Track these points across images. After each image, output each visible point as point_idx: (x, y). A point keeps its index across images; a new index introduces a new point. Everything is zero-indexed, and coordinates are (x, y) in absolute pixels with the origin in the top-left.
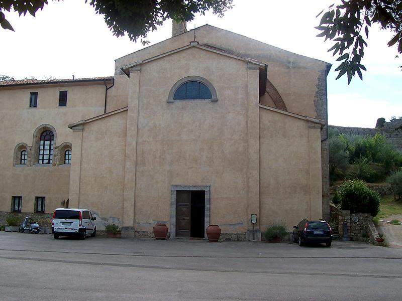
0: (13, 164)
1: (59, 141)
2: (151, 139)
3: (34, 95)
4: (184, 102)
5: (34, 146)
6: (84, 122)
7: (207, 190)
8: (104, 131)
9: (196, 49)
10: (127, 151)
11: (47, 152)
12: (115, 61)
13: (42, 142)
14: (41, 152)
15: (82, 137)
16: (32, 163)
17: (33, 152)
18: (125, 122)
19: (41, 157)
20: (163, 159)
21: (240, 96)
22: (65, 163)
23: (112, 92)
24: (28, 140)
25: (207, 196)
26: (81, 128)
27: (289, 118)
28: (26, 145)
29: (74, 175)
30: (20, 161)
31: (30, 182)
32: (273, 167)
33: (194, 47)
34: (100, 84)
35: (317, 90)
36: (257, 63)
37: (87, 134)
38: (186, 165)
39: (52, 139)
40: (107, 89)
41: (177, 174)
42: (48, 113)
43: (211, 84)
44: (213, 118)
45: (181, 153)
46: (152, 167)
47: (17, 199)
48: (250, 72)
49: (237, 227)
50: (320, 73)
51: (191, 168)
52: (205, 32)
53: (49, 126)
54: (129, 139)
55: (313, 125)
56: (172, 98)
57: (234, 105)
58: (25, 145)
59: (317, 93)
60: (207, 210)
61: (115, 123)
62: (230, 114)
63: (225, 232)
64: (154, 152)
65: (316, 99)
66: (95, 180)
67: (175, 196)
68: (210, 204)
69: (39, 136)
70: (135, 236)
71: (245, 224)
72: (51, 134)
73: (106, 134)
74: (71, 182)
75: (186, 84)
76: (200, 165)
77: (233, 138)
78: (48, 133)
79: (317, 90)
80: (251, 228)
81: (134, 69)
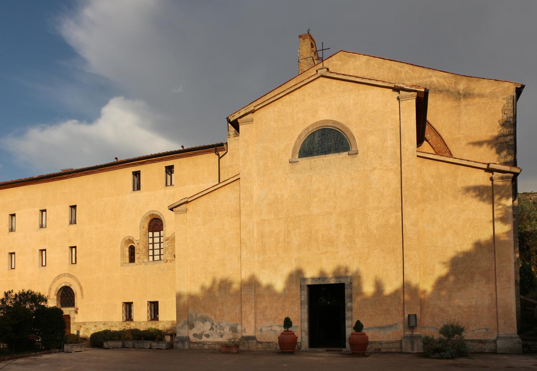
4: (312, 160)
6: (186, 200)
8: (213, 211)
13: (151, 234)
14: (151, 247)
21: (389, 143)
24: (136, 230)
25: (347, 292)
28: (133, 238)
30: (132, 259)
32: (439, 245)
34: (210, 152)
40: (220, 158)
43: (347, 129)
44: (352, 179)
47: (128, 306)
50: (505, 102)
52: (339, 63)
54: (244, 219)
56: (297, 156)
58: (131, 239)
60: (348, 311)
61: (227, 195)
62: (376, 171)
63: (373, 340)
64: (277, 234)
67: (305, 293)
68: (352, 302)
71: (401, 327)
75: (313, 134)
80: (408, 333)
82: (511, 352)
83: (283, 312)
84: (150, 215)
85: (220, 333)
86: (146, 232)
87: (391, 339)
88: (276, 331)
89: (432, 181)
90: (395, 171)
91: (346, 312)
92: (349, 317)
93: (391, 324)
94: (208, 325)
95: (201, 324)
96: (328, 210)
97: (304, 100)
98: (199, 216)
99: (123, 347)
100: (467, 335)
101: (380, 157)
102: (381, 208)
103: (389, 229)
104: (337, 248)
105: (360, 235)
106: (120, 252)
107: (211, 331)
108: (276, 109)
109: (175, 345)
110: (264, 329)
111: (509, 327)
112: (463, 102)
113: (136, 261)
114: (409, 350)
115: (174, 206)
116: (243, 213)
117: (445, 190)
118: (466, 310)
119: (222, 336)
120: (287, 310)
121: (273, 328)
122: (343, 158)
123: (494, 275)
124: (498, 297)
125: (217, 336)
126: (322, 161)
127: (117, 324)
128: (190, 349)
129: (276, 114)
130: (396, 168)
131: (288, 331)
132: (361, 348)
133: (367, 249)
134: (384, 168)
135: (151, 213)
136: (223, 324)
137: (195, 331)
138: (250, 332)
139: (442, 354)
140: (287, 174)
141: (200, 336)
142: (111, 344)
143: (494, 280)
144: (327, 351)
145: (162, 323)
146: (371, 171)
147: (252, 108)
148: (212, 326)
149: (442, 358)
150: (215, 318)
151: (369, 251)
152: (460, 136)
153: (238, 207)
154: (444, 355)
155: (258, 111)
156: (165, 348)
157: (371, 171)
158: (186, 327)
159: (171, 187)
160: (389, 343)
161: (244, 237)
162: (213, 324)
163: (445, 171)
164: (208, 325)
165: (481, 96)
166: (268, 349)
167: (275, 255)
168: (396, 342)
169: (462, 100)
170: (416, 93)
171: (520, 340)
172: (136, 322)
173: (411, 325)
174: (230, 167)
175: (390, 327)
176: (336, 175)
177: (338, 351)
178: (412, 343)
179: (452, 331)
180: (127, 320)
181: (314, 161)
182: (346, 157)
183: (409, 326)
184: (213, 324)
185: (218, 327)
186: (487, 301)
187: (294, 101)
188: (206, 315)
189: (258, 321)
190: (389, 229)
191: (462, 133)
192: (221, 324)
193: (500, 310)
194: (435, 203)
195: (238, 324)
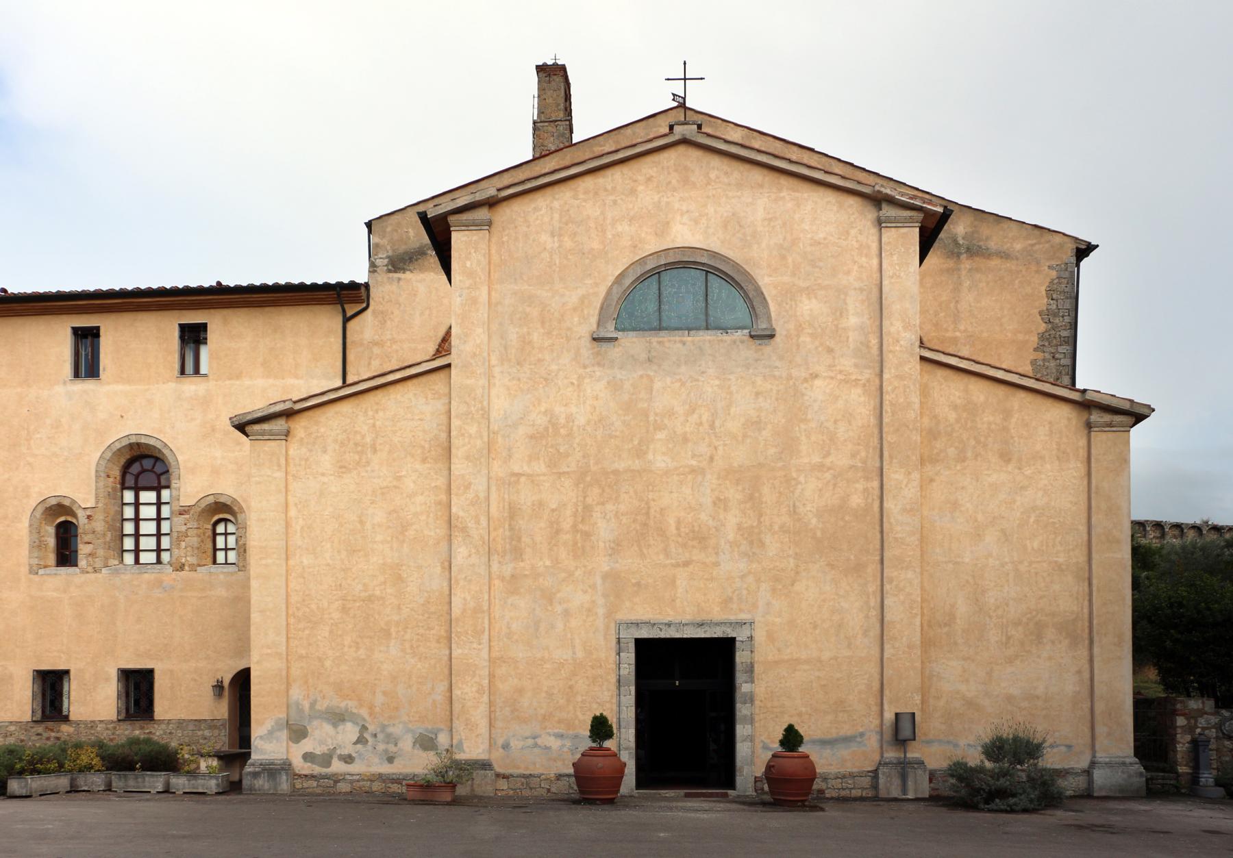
0: (31, 566)
1: (191, 486)
2: (540, 467)
3: (87, 338)
4: (654, 340)
5: (100, 505)
6: (288, 405)
7: (741, 635)
8: (368, 440)
9: (695, 153)
10: (454, 510)
11: (148, 528)
12: (369, 225)
13: (129, 496)
15: (286, 460)
16: (98, 563)
17: (99, 525)
18: (443, 409)
19: (129, 544)
20: (587, 535)
21: (853, 320)
22: (214, 562)
23: (365, 327)
24: (82, 487)
25: (741, 657)
26: (279, 425)
27: (1022, 394)
28: (74, 502)
29: (265, 595)
30: (66, 555)
31: (99, 626)
32: (967, 560)
33: (685, 141)
35: (1043, 327)
36: (918, 203)
37: (304, 450)
38: (667, 555)
39: (163, 483)
40: (346, 320)
41: (638, 584)
42: (141, 391)
43: (746, 274)
44: (757, 394)
45: (647, 514)
46: (548, 563)
47: (51, 685)
48: (889, 235)
49: (844, 752)
50: (1054, 274)
51: (687, 564)
53: (152, 442)
54: (459, 467)
55: (1107, 418)
57: (830, 351)
58: (67, 503)
59: (1042, 337)
62: (818, 382)
64: (553, 510)
65: (1040, 355)
66: (344, 610)
67: (630, 657)
68: (752, 682)
69: (116, 472)
70: (109, 789)
71: (873, 742)
72: (158, 469)
73: (375, 451)
74: (255, 617)
76: (717, 554)
77: (828, 461)
78: (147, 463)
79: (1043, 327)
80: (891, 754)
81: (465, 217)
82: (1124, 795)
83: (568, 701)
84: (131, 446)
85: (386, 751)
86: (114, 489)
87: (850, 768)
88: (547, 748)
89: (952, 416)
90: (864, 385)
91: (738, 706)
92: (745, 716)
93: (849, 733)
94: (350, 732)
95: (328, 728)
96: (694, 463)
97: (633, 192)
98: (325, 452)
99: (74, 790)
100: (1051, 760)
101: (830, 351)
102: (829, 469)
103: (847, 518)
104: (717, 554)
105: (776, 528)
106: (22, 534)
107: (359, 746)
108: (556, 204)
109: (246, 782)
110: (515, 744)
111: (1118, 742)
112: (966, 264)
113: (82, 563)
114: (895, 792)
115: (249, 417)
116: (458, 453)
117: (982, 439)
118: (1025, 704)
119: (391, 760)
120: (579, 699)
121: (539, 741)
122: (735, 342)
123: (1087, 631)
124: (1096, 678)
125: (377, 760)
126: (679, 345)
127: (12, 728)
128: (294, 791)
129: (556, 216)
130: (868, 380)
131: (601, 749)
132: (791, 787)
133: (792, 560)
134: (839, 377)
135: (133, 440)
136: (396, 730)
137: (307, 745)
138: (473, 750)
139: (1012, 801)
140: (585, 367)
141: (326, 759)
142: (35, 783)
143: (1087, 642)
144: (687, 795)
145: (163, 726)
146: (806, 380)
147: (492, 192)
148: (361, 733)
149: (1012, 811)
150: (371, 714)
151: (797, 566)
152: (958, 334)
153: (444, 435)
154: (1015, 804)
155: (505, 204)
156: (215, 791)
157: (806, 380)
158: (284, 734)
159: (196, 379)
160: (844, 777)
161: (461, 514)
162: (364, 728)
163: (982, 398)
164: (350, 732)
165: (1005, 256)
166: (526, 793)
167: (548, 563)
168: (861, 775)
169: (963, 257)
170: (920, 216)
171: (1142, 769)
172: (78, 723)
173: (901, 737)
174: (376, 344)
175: (847, 740)
176: (717, 382)
177: (717, 795)
178: (904, 777)
179: (1013, 750)
180: (45, 718)
181: (659, 343)
182: (742, 342)
183: (897, 740)
184: (364, 728)
185: (380, 736)
186: (1071, 685)
187: (606, 190)
188: (343, 705)
189: (499, 724)
190: (847, 518)
191: (962, 328)
192: (390, 730)
193: (1100, 707)
194: (958, 468)
195: (440, 730)
